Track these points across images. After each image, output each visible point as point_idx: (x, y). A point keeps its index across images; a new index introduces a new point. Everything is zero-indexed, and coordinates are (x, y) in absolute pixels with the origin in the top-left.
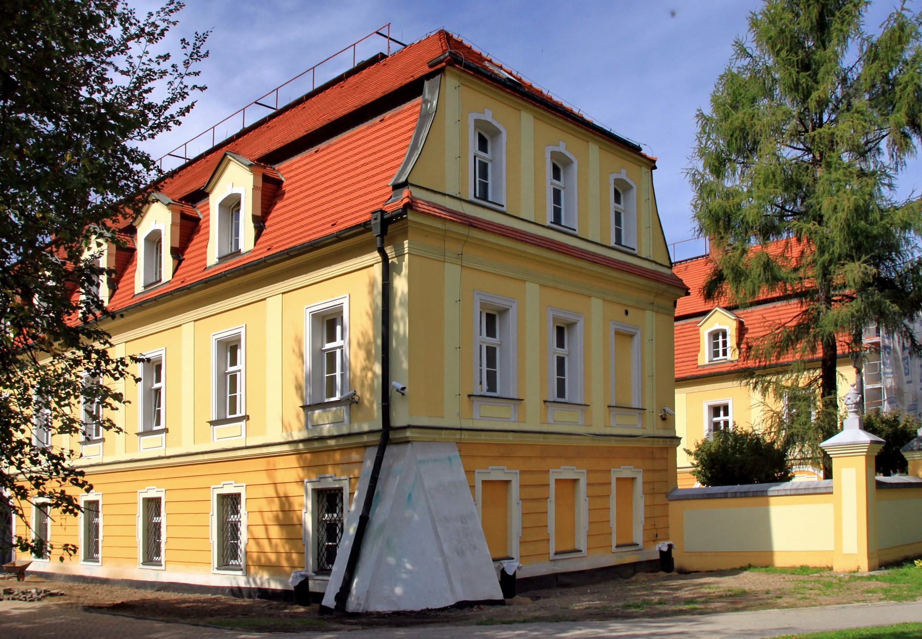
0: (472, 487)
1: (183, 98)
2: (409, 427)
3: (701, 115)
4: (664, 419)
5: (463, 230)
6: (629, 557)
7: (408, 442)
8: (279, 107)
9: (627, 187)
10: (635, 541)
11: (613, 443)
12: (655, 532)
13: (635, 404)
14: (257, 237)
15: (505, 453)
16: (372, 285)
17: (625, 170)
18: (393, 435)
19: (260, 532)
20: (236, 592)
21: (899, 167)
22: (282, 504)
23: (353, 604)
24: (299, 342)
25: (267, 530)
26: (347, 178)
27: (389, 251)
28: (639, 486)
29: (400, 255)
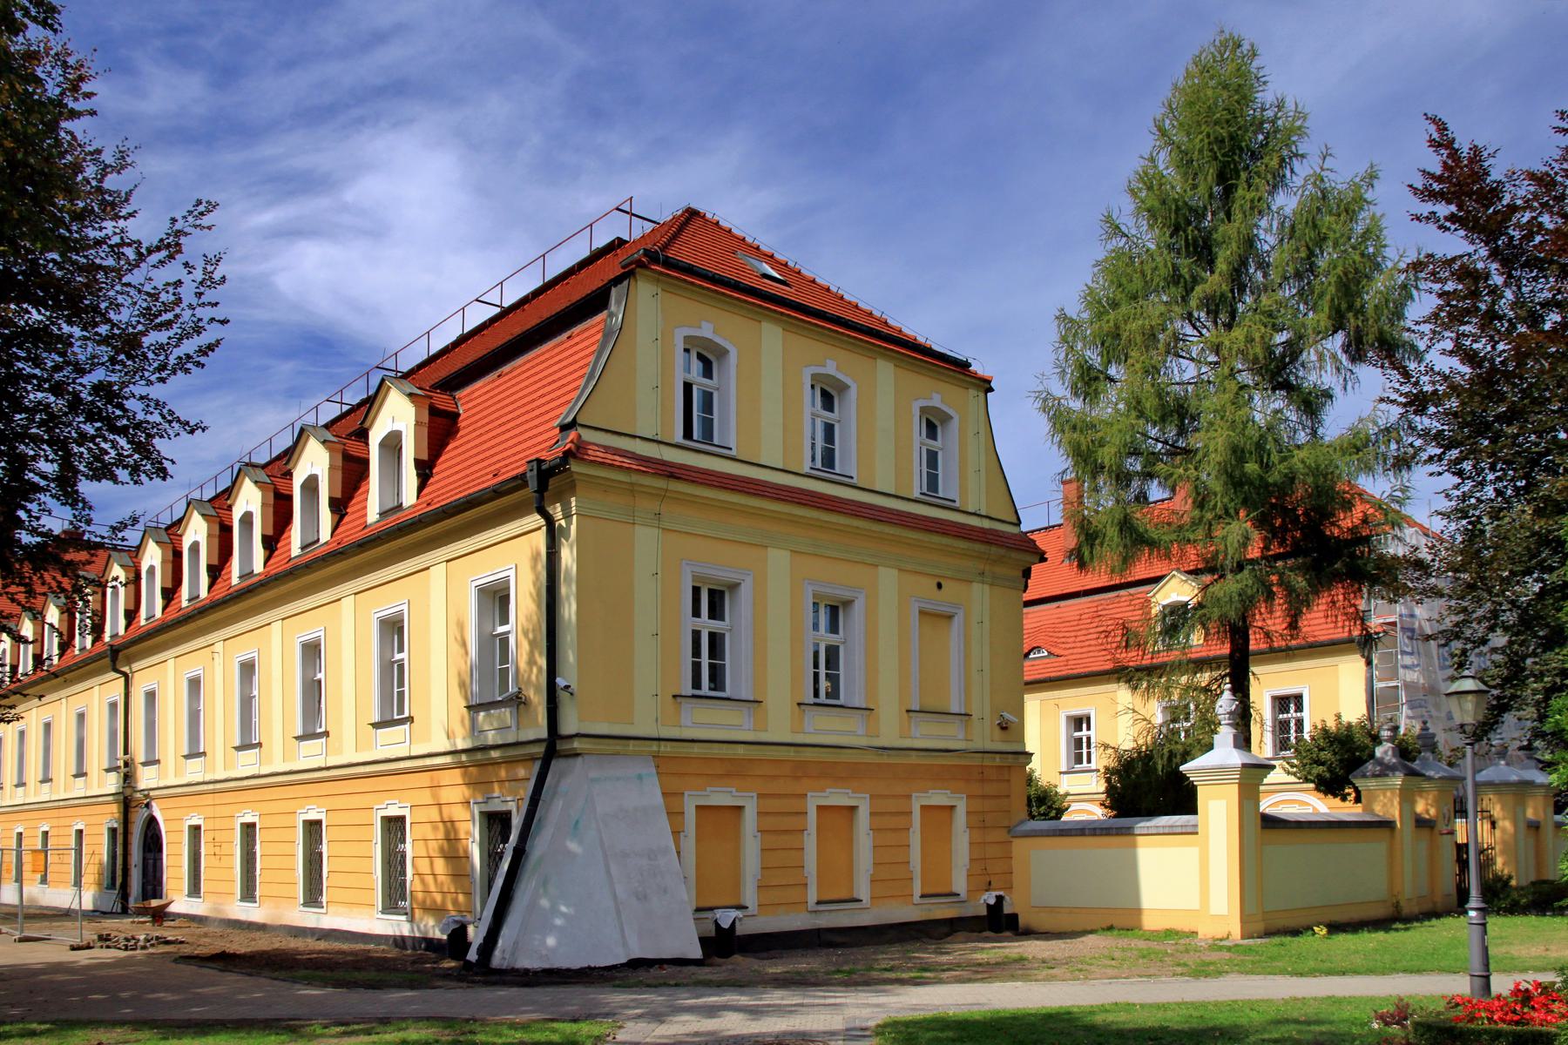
0: (675, 814)
1: (199, 333)
2: (577, 735)
3: (1063, 317)
4: (1004, 728)
5: (660, 483)
6: (942, 911)
7: (577, 755)
8: (506, 304)
9: (946, 418)
10: (955, 889)
11: (913, 759)
12: (982, 876)
13: (955, 709)
14: (421, 488)
15: (733, 771)
16: (535, 558)
17: (941, 394)
18: (562, 746)
19: (424, 866)
20: (400, 942)
21: (1350, 385)
22: (447, 832)
23: (497, 960)
24: (461, 626)
25: (432, 864)
26: (513, 419)
27: (557, 511)
28: (863, 818)
29: (567, 516)
